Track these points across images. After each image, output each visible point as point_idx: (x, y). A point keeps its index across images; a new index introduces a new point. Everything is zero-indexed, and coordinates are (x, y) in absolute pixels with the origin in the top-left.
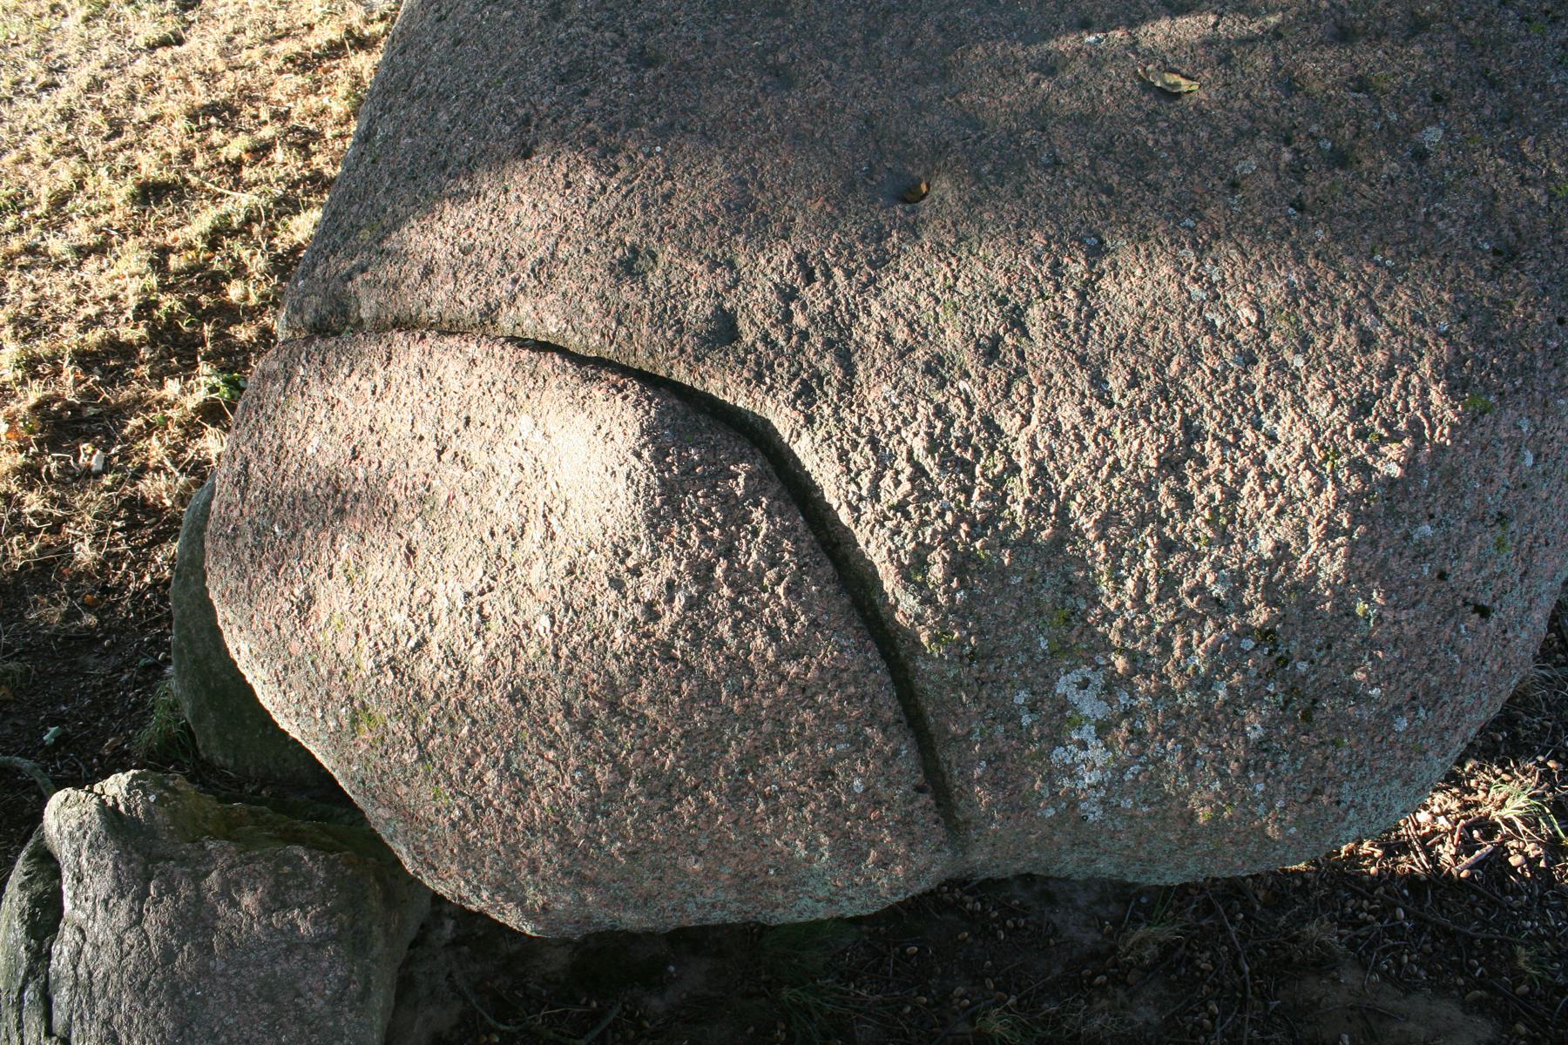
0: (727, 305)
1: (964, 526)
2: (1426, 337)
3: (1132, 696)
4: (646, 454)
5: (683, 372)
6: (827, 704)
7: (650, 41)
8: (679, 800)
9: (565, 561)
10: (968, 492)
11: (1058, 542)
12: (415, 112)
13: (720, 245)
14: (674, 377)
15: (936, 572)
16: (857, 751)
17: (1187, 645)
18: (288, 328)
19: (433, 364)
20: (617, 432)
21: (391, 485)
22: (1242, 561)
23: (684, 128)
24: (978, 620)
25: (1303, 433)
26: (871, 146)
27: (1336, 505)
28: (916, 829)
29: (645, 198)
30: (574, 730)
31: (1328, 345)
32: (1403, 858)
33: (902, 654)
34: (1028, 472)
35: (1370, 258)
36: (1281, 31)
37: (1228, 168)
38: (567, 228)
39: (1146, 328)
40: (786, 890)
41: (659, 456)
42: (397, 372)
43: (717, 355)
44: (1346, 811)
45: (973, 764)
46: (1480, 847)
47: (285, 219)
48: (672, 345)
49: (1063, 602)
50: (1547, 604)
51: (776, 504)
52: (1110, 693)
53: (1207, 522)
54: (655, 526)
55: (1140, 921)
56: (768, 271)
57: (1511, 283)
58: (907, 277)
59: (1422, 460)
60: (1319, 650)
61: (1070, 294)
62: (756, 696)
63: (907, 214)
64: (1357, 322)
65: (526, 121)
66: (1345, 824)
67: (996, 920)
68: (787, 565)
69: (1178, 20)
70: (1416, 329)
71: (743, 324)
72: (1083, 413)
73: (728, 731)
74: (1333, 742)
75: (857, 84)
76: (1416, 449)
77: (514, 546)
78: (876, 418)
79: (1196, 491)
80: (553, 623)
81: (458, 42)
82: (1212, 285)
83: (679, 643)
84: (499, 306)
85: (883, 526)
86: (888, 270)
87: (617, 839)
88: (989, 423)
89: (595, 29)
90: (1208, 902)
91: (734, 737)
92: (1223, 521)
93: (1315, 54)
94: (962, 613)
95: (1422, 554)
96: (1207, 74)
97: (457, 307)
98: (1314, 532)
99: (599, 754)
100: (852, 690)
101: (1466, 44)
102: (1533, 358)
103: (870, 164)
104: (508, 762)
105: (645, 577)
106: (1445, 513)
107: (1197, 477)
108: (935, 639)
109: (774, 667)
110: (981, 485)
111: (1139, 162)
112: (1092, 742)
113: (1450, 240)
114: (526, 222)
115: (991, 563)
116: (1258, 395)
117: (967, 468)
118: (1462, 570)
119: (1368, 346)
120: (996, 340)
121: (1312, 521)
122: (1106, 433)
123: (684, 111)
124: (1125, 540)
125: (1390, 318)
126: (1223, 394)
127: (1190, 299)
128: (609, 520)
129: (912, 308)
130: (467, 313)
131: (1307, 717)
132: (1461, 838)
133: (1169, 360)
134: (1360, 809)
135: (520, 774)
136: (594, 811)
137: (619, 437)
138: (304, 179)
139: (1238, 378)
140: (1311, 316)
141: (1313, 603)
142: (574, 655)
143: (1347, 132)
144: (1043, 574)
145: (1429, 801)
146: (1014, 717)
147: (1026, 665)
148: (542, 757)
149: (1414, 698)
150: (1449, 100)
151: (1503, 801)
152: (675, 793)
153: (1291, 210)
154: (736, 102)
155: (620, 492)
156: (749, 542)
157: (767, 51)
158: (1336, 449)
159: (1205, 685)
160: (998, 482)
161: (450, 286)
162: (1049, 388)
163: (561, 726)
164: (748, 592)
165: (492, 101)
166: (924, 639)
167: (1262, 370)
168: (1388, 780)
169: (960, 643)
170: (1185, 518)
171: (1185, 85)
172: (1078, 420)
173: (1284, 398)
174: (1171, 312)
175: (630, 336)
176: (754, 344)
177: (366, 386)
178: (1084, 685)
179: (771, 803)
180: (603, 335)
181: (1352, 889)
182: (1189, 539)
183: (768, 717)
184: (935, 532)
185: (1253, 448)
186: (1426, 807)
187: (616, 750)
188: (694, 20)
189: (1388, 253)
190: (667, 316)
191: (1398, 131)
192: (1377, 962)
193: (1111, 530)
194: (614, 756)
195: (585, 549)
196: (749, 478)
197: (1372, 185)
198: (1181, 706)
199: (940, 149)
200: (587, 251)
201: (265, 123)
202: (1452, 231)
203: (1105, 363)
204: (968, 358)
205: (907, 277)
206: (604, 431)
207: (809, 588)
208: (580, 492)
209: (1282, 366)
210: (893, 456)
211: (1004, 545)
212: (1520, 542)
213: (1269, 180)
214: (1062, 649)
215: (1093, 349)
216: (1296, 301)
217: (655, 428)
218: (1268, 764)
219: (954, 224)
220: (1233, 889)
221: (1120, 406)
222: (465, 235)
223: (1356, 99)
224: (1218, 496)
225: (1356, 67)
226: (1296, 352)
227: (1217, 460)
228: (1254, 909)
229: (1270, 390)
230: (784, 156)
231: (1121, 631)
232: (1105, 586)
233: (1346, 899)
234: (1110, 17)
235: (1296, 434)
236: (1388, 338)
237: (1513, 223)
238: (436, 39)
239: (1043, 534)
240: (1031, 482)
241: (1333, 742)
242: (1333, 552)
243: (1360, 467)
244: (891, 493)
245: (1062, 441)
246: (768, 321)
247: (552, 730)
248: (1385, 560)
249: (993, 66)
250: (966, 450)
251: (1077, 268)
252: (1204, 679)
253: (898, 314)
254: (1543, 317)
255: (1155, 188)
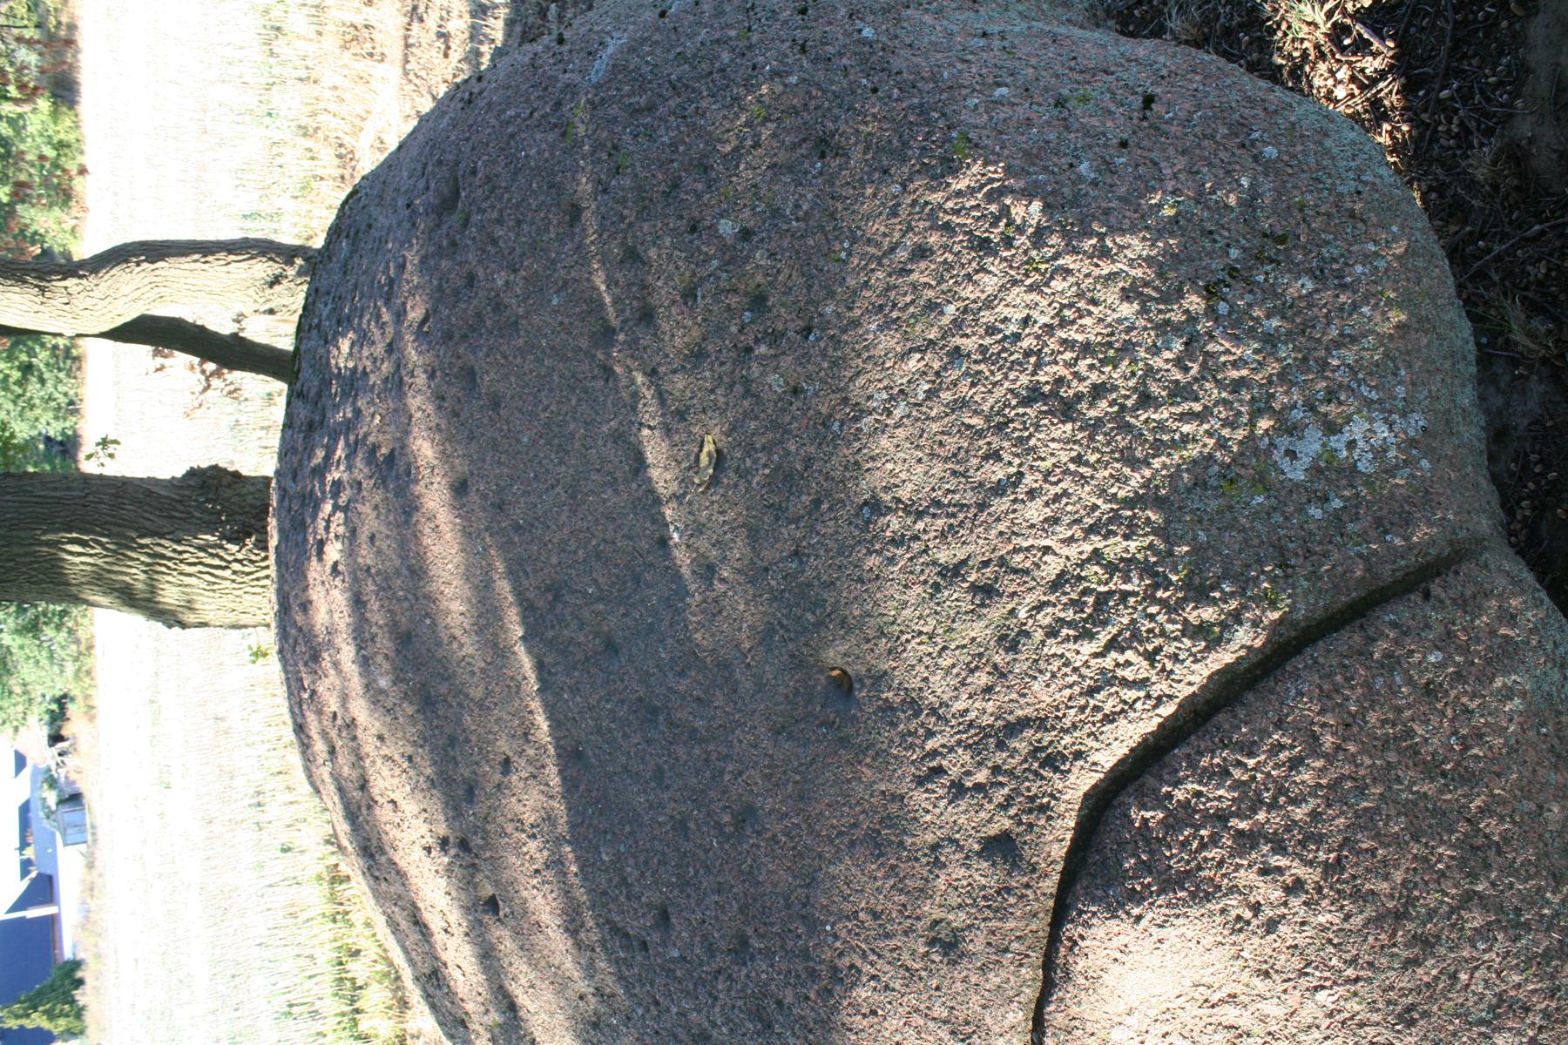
0: (976, 847)
1: (1159, 594)
2: (909, 201)
3: (1294, 406)
4: (1136, 911)
5: (1048, 882)
6: (1358, 700)
7: (723, 944)
8: (1486, 836)
9: (1256, 981)
10: (1125, 595)
11: (1159, 503)
13: (917, 859)
14: (1054, 891)
15: (1208, 614)
16: (1399, 663)
17: (1235, 365)
20: (1117, 942)
22: (1145, 328)
23: (805, 906)
24: (1248, 566)
28: (1468, 593)
29: (878, 937)
30: (1433, 954)
32: (1386, 102)
33: (1293, 634)
34: (1097, 542)
36: (649, 370)
37: (780, 399)
38: (917, 1010)
40: (1560, 713)
41: (1136, 897)
43: (1027, 852)
44: (1365, 183)
45: (1391, 548)
46: (1360, 35)
48: (1023, 896)
49: (1216, 488)
51: (1166, 777)
52: (1295, 428)
54: (1207, 894)
55: (1508, 341)
56: (937, 811)
58: (926, 679)
59: (1021, 184)
60: (1215, 241)
61: (920, 525)
62: (1362, 772)
63: (863, 685)
64: (905, 263)
66: (1378, 181)
67: (1537, 483)
68: (1225, 759)
69: (649, 461)
70: (903, 212)
71: (993, 830)
72: (1032, 499)
73: (1403, 796)
74: (1301, 210)
76: (1012, 192)
77: (1248, 1035)
78: (1067, 692)
79: (1088, 382)
80: (1323, 987)
82: (892, 398)
83: (1322, 856)
85: (1172, 672)
86: (921, 698)
87: (1543, 897)
88: (1056, 584)
89: (716, 999)
90: (1471, 279)
91: (1409, 789)
92: (1111, 353)
94: (1244, 584)
95: (1108, 166)
96: (695, 429)
98: (1106, 268)
99: (1453, 925)
100: (1338, 677)
101: (644, 213)
103: (821, 725)
104: (1481, 1022)
105: (1260, 898)
106: (1066, 155)
107: (1074, 383)
108: (1273, 605)
109: (1330, 758)
110: (1116, 583)
111: (786, 479)
112: (1346, 437)
115: (1190, 563)
116: (988, 341)
117: (1102, 599)
118: (1116, 128)
120: (975, 588)
121: (1097, 272)
122: (1048, 473)
123: (788, 907)
125: (897, 235)
126: (992, 373)
127: (908, 416)
128: (1208, 941)
129: (955, 671)
131: (1282, 240)
132: (1354, 54)
133: (969, 427)
134: (1360, 171)
135: (1492, 1008)
136: (1518, 925)
137: (1123, 939)
139: (976, 362)
141: (1172, 255)
142: (1353, 962)
143: (733, 300)
144: (1192, 512)
145: (1323, 90)
146: (1337, 516)
147: (1283, 513)
148: (1468, 986)
149: (1243, 146)
151: (1309, 24)
152: (1480, 841)
153: (811, 338)
154: (774, 858)
155: (1178, 932)
156: (1209, 800)
157: (722, 833)
158: (1026, 263)
159: (1270, 340)
160: (1111, 568)
162: (1014, 533)
163: (1429, 970)
164: (1258, 793)
166: (1276, 615)
167: (964, 340)
168: (1328, 152)
169: (1273, 580)
170: (1115, 388)
171: (709, 447)
172: (1039, 502)
173: (986, 317)
176: (1010, 817)
178: (1291, 454)
179: (1470, 741)
180: (1021, 965)
181: (1430, 143)
182: (1134, 381)
183: (1382, 758)
184: (1170, 621)
185: (1038, 337)
186: (1330, 92)
187: (1445, 908)
188: (698, 905)
190: (995, 904)
192: (1502, 105)
193: (1138, 454)
194: (1453, 910)
195: (1241, 962)
196: (1144, 807)
198: (1295, 359)
199: (797, 663)
200: (938, 988)
202: (809, 196)
203: (981, 484)
204: (996, 612)
205: (926, 679)
206: (1118, 955)
207: (1245, 735)
208: (1184, 973)
209: (957, 324)
210: (1103, 671)
211: (1170, 553)
213: (786, 362)
214: (1261, 481)
215: (969, 498)
217: (1109, 905)
218: (1335, 266)
219: (868, 641)
220: (1456, 254)
221: (1020, 465)
223: (704, 297)
224: (1089, 361)
225: (674, 302)
226: (942, 313)
227: (1055, 368)
228: (1471, 233)
229: (981, 331)
231: (1234, 429)
232: (1193, 451)
233: (1442, 147)
234: (654, 521)
235: (1019, 300)
237: (795, 146)
239: (1153, 518)
240: (1105, 537)
241: (1301, 210)
243: (1039, 238)
244: (1139, 668)
245: (1061, 514)
246: (987, 806)
247: (1436, 978)
248: (1120, 199)
249: (711, 621)
250: (1085, 603)
251: (894, 523)
252: (1265, 342)
253: (963, 684)
254: (874, 105)
255: (808, 461)
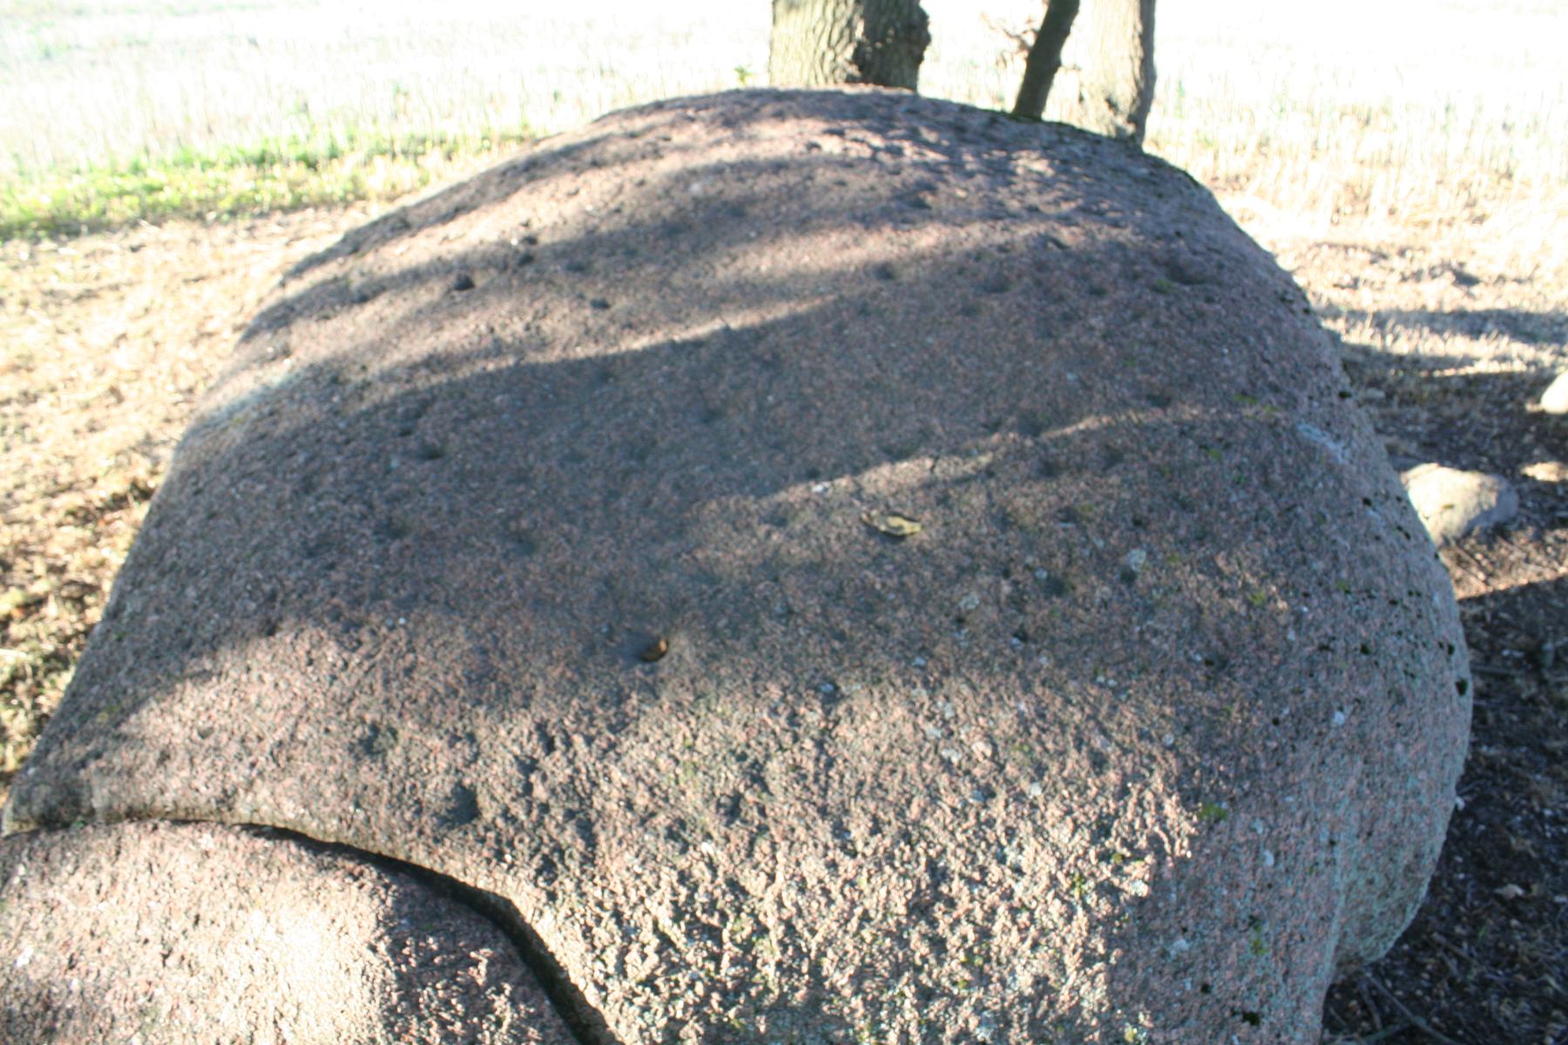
0: (467, 782)
2: (1155, 752)
7: (398, 512)
10: (716, 958)
11: (814, 1002)
12: (164, 588)
13: (461, 718)
14: (414, 860)
18: (15, 820)
19: (164, 858)
20: (352, 927)
21: (109, 997)
22: (1003, 1000)
23: (428, 598)
25: (1047, 863)
26: (611, 608)
27: (1089, 932)
29: (386, 672)
31: (1062, 770)
34: (777, 932)
35: (1093, 680)
37: (953, 604)
38: (307, 707)
39: (884, 772)
41: (396, 949)
42: (125, 867)
43: (456, 834)
47: (53, 676)
48: (411, 826)
50: (1314, 1000)
51: (521, 989)
53: (963, 964)
57: (1225, 690)
58: (646, 740)
59: (1167, 874)
61: (808, 744)
63: (647, 674)
65: (272, 597)
70: (1144, 746)
71: (483, 800)
75: (597, 547)
78: (619, 890)
79: (948, 934)
81: (212, 516)
82: (945, 722)
84: (236, 792)
88: (734, 886)
92: (978, 961)
93: (1025, 489)
95: (1182, 969)
96: (927, 515)
97: (192, 794)
98: (1071, 961)
101: (1157, 471)
102: (1256, 761)
103: (610, 626)
106: (1197, 925)
110: (730, 951)
111: (868, 606)
113: (1165, 655)
114: (267, 703)
115: (747, 1032)
116: (1000, 829)
117: (714, 934)
118: (1223, 981)
119: (1101, 766)
120: (737, 798)
121: (1068, 950)
122: (852, 883)
123: (428, 581)
124: (882, 993)
125: (1119, 737)
126: (965, 831)
127: (925, 739)
128: (343, 1022)
129: (652, 771)
130: (203, 800)
133: (909, 802)
137: (353, 929)
138: (77, 633)
139: (978, 814)
140: (1042, 744)
141: (1081, 1036)
143: (1060, 561)
150: (1149, 523)
153: (1015, 641)
154: (479, 570)
156: (492, 1034)
157: (510, 518)
158: (1081, 875)
160: (747, 946)
161: (185, 773)
162: (792, 843)
165: (240, 577)
167: (1001, 804)
170: (940, 962)
171: (908, 527)
173: (1025, 828)
174: (908, 753)
175: (368, 820)
177: (91, 885)
180: (341, 820)
182: (947, 984)
184: (686, 1006)
185: (1000, 883)
189: (1111, 673)
190: (406, 799)
191: (1106, 556)
196: (491, 963)
197: (1087, 610)
199: (676, 607)
200: (327, 731)
201: (38, 578)
202: (1166, 647)
203: (847, 812)
204: (711, 820)
206: (338, 924)
209: (1020, 797)
211: (759, 1011)
212: (1276, 942)
213: (991, 613)
215: (833, 798)
216: (1027, 730)
219: (692, 681)
221: (864, 855)
222: (204, 718)
223: (1065, 530)
226: (1032, 781)
227: (965, 898)
229: (1010, 823)
230: (526, 623)
234: (836, 467)
236: (1119, 757)
237: (1220, 633)
238: (192, 513)
240: (781, 942)
242: (1092, 979)
244: (638, 968)
245: (811, 895)
248: (1146, 982)
249: (727, 520)
250: (712, 915)
253: (639, 779)
254: (1259, 720)
255: (885, 630)
